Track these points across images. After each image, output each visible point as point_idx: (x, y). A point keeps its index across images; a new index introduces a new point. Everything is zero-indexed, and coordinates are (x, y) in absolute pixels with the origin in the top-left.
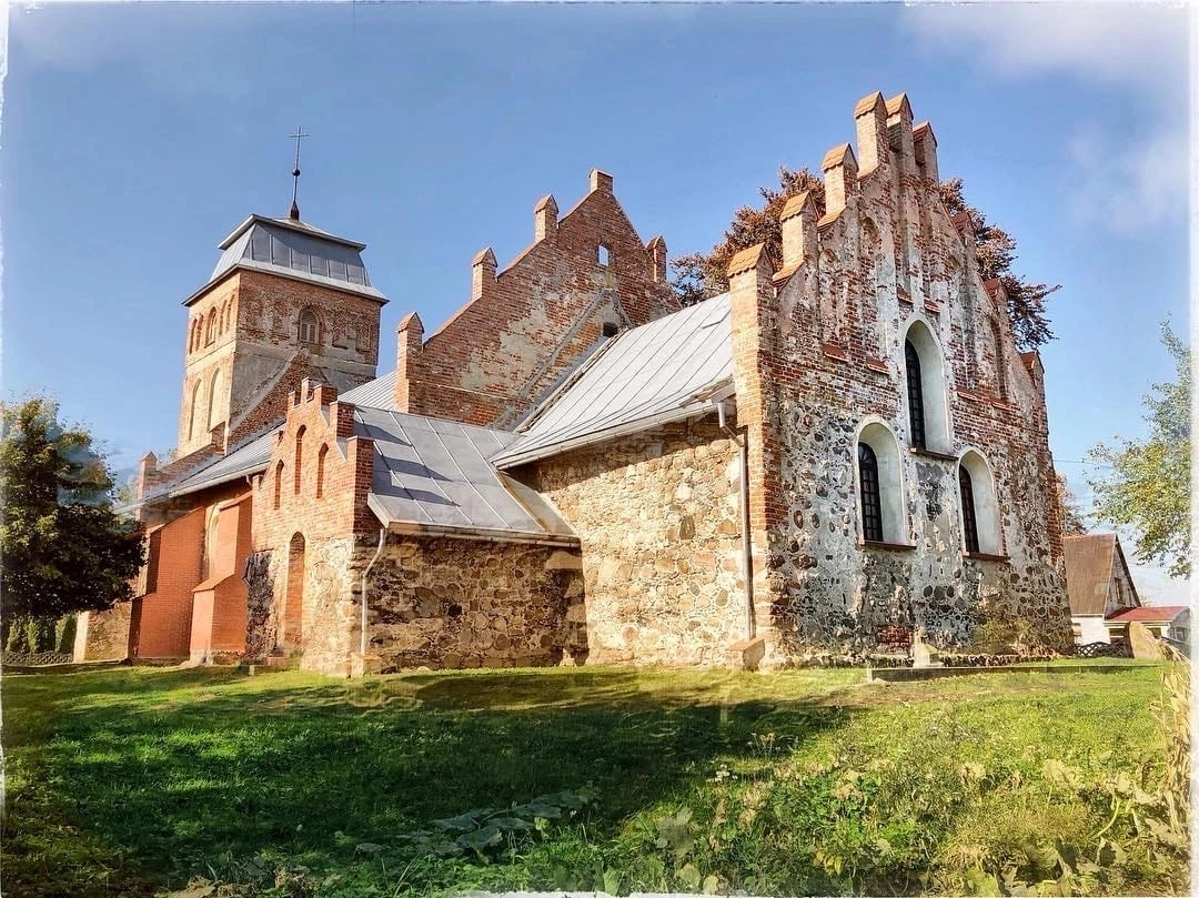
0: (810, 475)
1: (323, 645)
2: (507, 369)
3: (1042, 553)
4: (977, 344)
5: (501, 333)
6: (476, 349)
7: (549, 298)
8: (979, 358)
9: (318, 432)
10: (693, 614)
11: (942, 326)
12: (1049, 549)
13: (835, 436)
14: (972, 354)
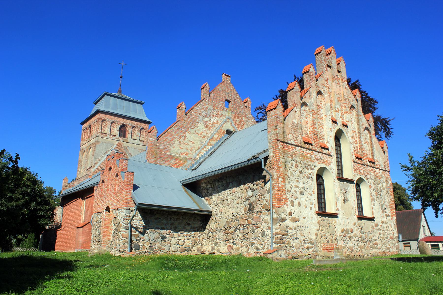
0: (298, 187)
1: (115, 248)
2: (189, 147)
3: (387, 216)
4: (362, 137)
5: (187, 133)
6: (177, 139)
7: (205, 120)
8: (363, 143)
9: (115, 169)
10: (252, 240)
11: (349, 131)
12: (390, 214)
13: (307, 172)
14: (361, 141)
